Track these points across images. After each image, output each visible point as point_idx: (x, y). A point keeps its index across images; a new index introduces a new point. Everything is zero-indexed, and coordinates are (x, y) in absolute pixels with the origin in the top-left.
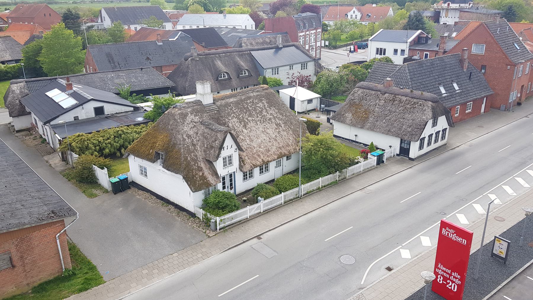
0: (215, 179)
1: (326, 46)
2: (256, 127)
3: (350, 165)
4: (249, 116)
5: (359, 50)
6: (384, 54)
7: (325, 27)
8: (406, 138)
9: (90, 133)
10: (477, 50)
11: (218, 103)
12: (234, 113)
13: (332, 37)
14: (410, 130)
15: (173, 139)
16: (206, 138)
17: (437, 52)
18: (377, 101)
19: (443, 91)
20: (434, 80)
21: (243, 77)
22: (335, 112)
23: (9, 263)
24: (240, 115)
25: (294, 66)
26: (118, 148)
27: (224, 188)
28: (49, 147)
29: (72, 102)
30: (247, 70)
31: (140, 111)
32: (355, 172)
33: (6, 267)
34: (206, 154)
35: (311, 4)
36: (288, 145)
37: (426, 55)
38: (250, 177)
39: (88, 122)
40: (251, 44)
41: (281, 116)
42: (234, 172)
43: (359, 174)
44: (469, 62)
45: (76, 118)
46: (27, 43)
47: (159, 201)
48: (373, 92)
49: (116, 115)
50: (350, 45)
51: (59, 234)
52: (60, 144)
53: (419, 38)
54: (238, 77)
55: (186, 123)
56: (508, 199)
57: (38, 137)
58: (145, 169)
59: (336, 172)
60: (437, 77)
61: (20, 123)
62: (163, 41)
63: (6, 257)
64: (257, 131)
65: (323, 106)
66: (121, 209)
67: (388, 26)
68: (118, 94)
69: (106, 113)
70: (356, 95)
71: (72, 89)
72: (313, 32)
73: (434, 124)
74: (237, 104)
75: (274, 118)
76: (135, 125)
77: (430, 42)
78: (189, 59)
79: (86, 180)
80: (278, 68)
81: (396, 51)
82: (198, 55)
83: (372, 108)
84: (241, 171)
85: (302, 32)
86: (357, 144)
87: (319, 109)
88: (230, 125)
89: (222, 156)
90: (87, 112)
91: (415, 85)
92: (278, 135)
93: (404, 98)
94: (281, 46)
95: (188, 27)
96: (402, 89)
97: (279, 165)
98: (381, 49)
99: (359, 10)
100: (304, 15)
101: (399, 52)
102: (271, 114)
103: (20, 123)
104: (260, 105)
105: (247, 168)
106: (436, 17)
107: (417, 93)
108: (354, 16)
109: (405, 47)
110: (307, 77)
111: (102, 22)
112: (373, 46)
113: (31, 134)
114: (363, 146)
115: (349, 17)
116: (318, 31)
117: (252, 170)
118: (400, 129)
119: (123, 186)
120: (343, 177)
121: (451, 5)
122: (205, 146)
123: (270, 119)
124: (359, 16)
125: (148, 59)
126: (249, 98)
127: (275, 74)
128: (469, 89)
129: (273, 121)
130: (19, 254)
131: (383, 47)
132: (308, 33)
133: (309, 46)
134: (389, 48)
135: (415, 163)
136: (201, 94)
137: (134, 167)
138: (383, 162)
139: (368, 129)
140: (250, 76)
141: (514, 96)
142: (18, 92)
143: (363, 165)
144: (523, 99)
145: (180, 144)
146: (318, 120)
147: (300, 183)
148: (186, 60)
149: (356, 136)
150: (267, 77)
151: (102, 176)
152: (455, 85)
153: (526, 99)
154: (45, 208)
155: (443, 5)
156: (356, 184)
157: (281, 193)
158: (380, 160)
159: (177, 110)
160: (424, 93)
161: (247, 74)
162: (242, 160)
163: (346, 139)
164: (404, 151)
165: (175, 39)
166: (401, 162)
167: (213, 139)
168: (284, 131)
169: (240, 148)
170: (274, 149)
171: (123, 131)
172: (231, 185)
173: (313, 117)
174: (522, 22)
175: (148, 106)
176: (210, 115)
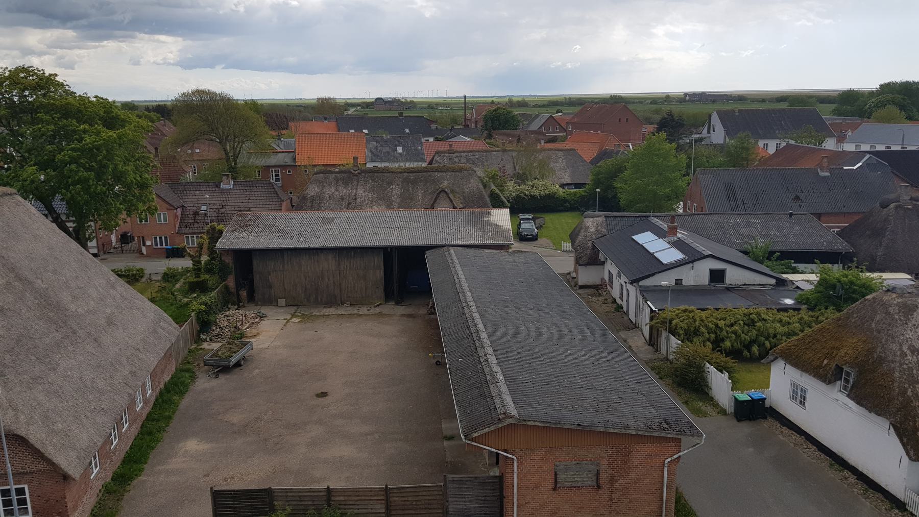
9: (703, 310)
15: (879, 349)
23: (594, 479)
26: (746, 343)
28: (626, 318)
29: (674, 255)
31: (786, 288)
33: (590, 483)
39: (696, 291)
45: (679, 282)
46: (594, 161)
47: (823, 456)
49: (744, 287)
51: (669, 460)
52: (652, 319)
55: (910, 325)
57: (610, 300)
58: (804, 391)
61: (587, 276)
62: (830, 170)
63: (593, 468)
66: (751, 450)
68: (745, 253)
69: (727, 281)
71: (675, 235)
76: (779, 310)
78: (892, 205)
79: (691, 383)
90: (697, 275)
95: (880, 148)
103: (587, 276)
111: (709, 132)
113: (600, 295)
119: (754, 411)
125: (797, 198)
127: (161, 238)
130: (610, 471)
137: (780, 383)
142: (593, 229)
145: (894, 362)
148: (884, 205)
151: (720, 384)
154: (654, 412)
159: (894, 296)
165: (855, 168)
171: (758, 314)
175: (806, 278)
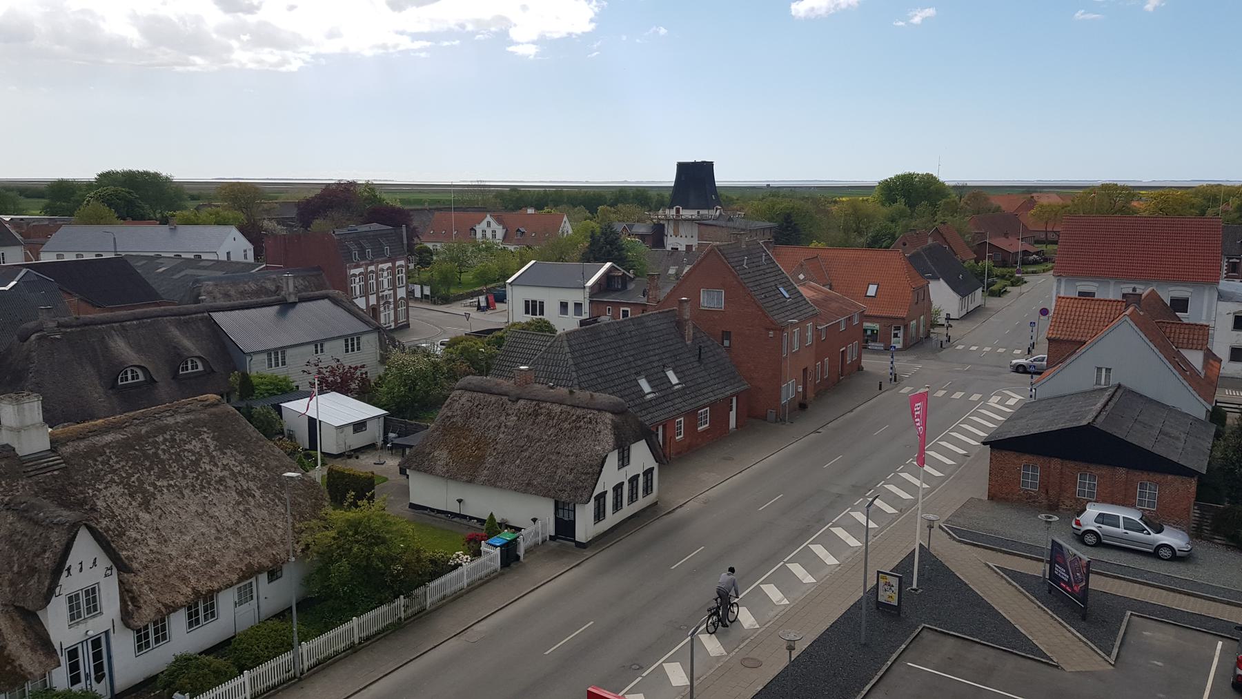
0: (43, 658)
1: (424, 297)
2: (180, 503)
3: (435, 575)
4: (158, 478)
5: (498, 305)
6: (542, 313)
7: (424, 259)
8: (564, 497)
10: (712, 300)
11: (67, 450)
12: (114, 471)
13: (436, 276)
14: (570, 477)
16: (17, 546)
17: (644, 308)
18: (503, 418)
19: (646, 387)
20: (626, 366)
21: (188, 376)
22: (411, 447)
24: (130, 476)
25: (327, 346)
27: (75, 680)
30: (199, 357)
32: (448, 591)
34: (14, 593)
35: (399, 205)
36: (271, 543)
37: (625, 313)
38: (157, 640)
40: (227, 295)
41: (253, 471)
42: (107, 633)
43: (458, 596)
44: (695, 327)
48: (493, 398)
50: (480, 293)
53: (607, 276)
54: (175, 376)
56: (772, 614)
59: (398, 597)
60: (631, 359)
64: (181, 512)
65: (392, 435)
67: (558, 253)
70: (456, 406)
72: (385, 266)
73: (624, 461)
74: (124, 448)
75: (234, 475)
77: (631, 286)
78: (33, 337)
80: (283, 349)
81: (564, 306)
82: (59, 325)
83: (491, 434)
84: (127, 625)
85: (357, 266)
86: (464, 521)
87: (380, 443)
88: (100, 504)
89: (64, 592)
91: (586, 378)
92: (242, 519)
93: (557, 409)
94: (292, 299)
96: (552, 388)
97: (246, 595)
98: (534, 302)
99: (499, 221)
100: (364, 228)
101: (571, 308)
102: (225, 467)
104: (196, 445)
105: (147, 614)
106: (657, 237)
107: (583, 395)
108: (489, 235)
109: (581, 296)
110: (356, 368)
112: (517, 297)
114: (478, 525)
115: (479, 235)
116: (398, 263)
117: (163, 620)
118: (551, 478)
120: (416, 608)
121: (682, 212)
122: (15, 569)
123: (221, 480)
124: (500, 233)
126: (163, 430)
127: (277, 365)
128: (700, 381)
129: (231, 483)
131: (538, 298)
132: (372, 268)
133: (378, 299)
134: (551, 299)
135: (588, 553)
136: (11, 429)
138: (518, 557)
139: (484, 484)
140: (209, 371)
141: (790, 390)
143: (467, 568)
144: (810, 395)
146: (377, 470)
147: (296, 639)
148: (24, 338)
149: (460, 501)
150: (254, 373)
152: (671, 375)
153: (816, 395)
155: (667, 212)
156: (446, 623)
157: (241, 673)
158: (509, 555)
160: (596, 395)
161: (201, 368)
162: (129, 599)
163: (439, 511)
164: (565, 528)
166: (559, 554)
167: (38, 548)
168: (259, 506)
169: (121, 566)
170: (230, 556)
172: (99, 668)
173: (365, 465)
174: (812, 246)
176: (37, 483)
